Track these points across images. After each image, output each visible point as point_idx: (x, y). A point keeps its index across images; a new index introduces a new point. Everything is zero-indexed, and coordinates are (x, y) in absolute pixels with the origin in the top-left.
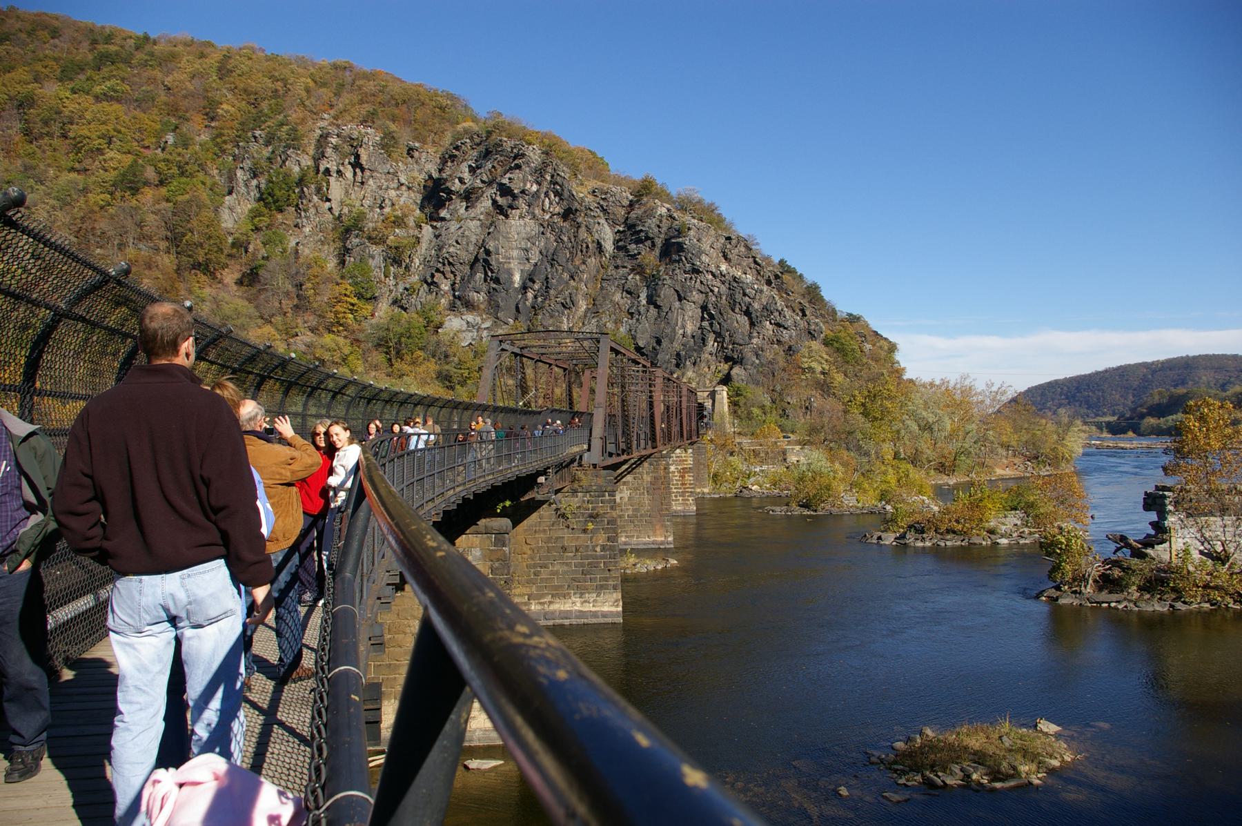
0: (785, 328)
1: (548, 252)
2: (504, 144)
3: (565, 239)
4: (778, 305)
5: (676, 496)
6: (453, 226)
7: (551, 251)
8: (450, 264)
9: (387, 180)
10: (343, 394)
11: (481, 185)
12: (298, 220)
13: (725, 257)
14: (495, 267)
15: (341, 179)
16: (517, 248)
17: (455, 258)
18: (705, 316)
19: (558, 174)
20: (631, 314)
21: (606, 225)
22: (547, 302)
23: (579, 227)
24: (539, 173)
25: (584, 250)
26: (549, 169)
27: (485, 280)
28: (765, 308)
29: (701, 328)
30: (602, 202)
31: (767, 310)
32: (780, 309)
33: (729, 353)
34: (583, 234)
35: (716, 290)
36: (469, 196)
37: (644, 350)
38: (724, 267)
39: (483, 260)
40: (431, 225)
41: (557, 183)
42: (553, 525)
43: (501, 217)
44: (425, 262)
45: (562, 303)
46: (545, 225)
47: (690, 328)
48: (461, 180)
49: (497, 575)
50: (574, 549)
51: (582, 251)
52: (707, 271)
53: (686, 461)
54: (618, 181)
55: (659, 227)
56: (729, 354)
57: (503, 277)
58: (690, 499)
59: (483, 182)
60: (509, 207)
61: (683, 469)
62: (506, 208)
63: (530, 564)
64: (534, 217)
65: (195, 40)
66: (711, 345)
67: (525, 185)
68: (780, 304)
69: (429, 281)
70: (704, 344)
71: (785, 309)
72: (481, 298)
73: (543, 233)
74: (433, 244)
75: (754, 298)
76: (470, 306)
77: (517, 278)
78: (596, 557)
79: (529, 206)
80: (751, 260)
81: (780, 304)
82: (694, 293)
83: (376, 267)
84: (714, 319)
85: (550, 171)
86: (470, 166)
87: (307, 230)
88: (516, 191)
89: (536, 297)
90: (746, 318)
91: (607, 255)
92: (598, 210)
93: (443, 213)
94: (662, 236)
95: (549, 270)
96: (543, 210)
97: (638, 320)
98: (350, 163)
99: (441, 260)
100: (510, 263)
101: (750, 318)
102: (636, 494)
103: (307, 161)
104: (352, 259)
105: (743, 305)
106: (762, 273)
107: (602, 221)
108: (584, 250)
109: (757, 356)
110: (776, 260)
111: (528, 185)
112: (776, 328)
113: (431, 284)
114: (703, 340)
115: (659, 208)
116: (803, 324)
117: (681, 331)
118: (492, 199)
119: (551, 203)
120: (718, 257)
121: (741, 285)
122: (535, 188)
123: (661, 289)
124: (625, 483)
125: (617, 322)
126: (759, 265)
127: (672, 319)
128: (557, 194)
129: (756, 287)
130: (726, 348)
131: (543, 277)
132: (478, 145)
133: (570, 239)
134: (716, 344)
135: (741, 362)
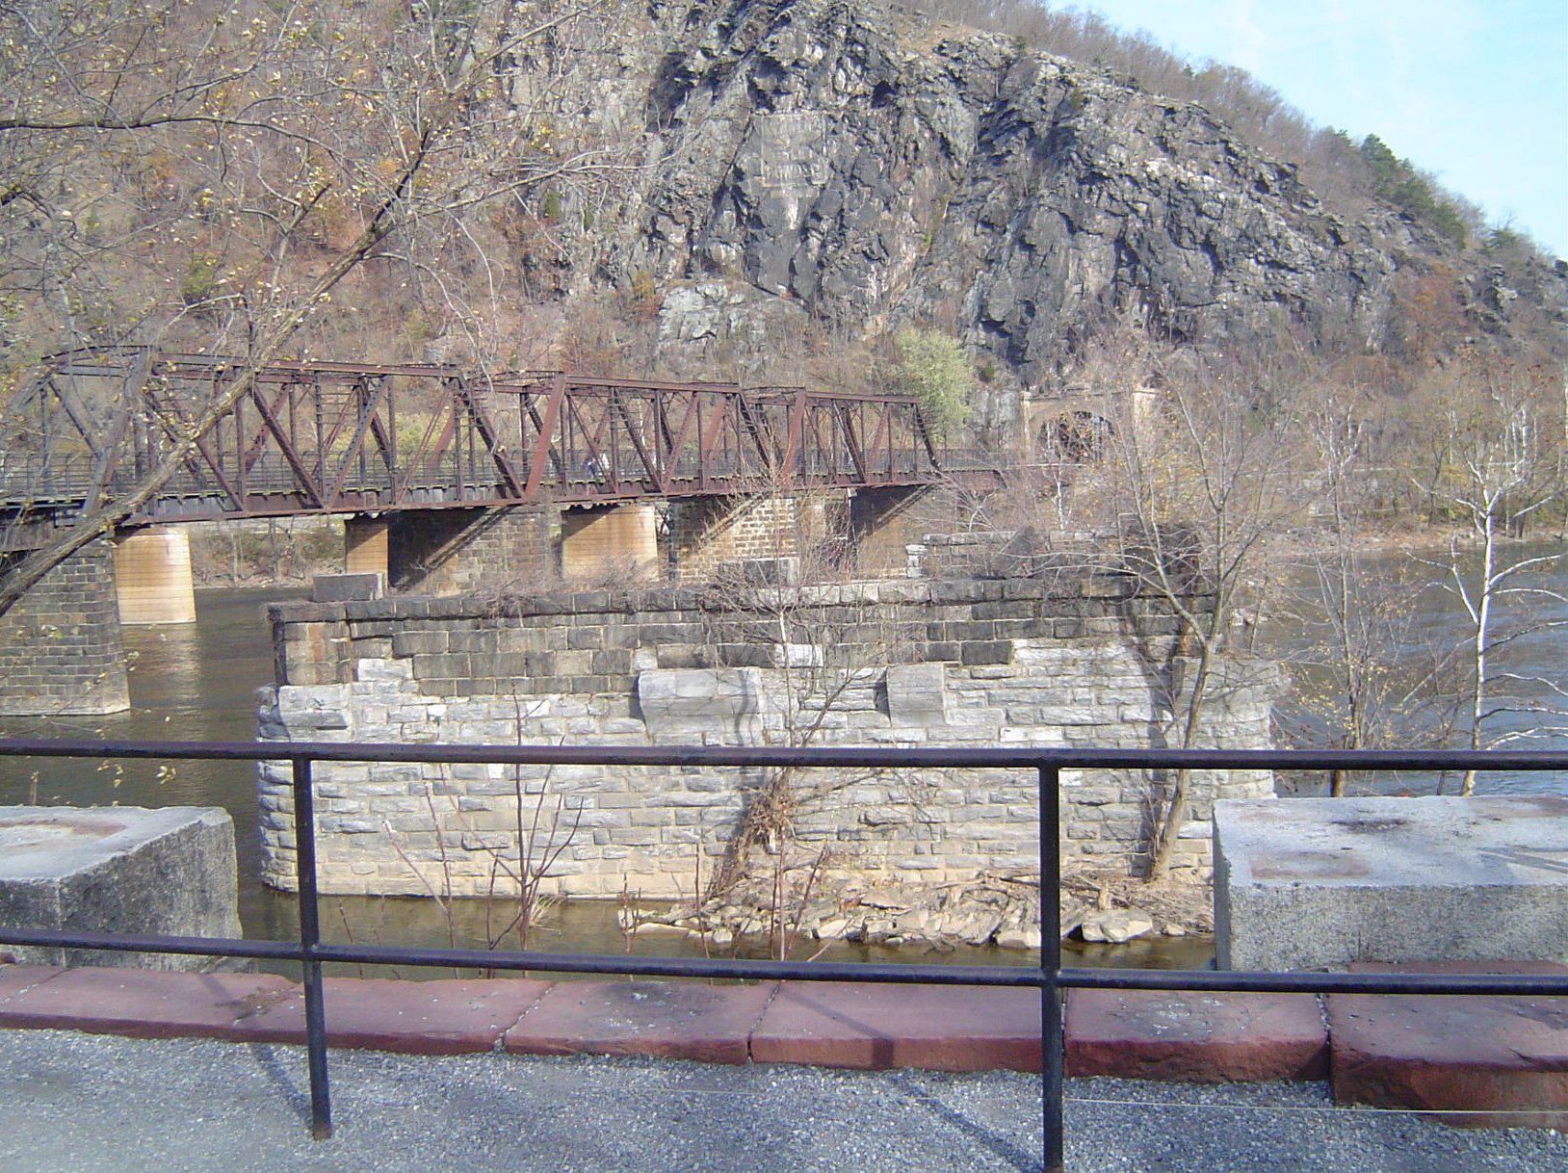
0: (1291, 270)
3: (876, 138)
4: (1270, 227)
6: (689, 131)
7: (850, 161)
13: (1164, 145)
18: (1123, 257)
19: (859, 26)
21: (958, 105)
24: (825, 27)
25: (911, 155)
26: (842, 18)
28: (1244, 235)
31: (1249, 238)
35: (1142, 208)
36: (715, 80)
37: (1005, 327)
39: (730, 191)
41: (856, 42)
45: (864, 253)
47: (1094, 280)
48: (706, 52)
52: (1121, 176)
55: (1041, 101)
57: (766, 214)
62: (770, 94)
66: (1135, 311)
67: (801, 50)
68: (1275, 223)
73: (834, 132)
76: (712, 266)
77: (793, 213)
79: (809, 86)
80: (1220, 146)
83: (571, 213)
84: (1139, 262)
85: (845, 21)
86: (721, 27)
88: (784, 64)
89: (823, 246)
90: (1207, 256)
91: (963, 160)
94: (1048, 118)
95: (847, 195)
96: (835, 90)
100: (779, 188)
101: (1214, 256)
105: (1197, 233)
106: (1241, 170)
108: (911, 155)
109: (1228, 325)
111: (808, 50)
117: (1077, 288)
119: (848, 78)
120: (1146, 147)
121: (1190, 195)
122: (819, 53)
124: (475, 553)
126: (1235, 156)
128: (857, 60)
129: (1222, 196)
131: (835, 208)
133: (883, 137)
134: (1146, 308)
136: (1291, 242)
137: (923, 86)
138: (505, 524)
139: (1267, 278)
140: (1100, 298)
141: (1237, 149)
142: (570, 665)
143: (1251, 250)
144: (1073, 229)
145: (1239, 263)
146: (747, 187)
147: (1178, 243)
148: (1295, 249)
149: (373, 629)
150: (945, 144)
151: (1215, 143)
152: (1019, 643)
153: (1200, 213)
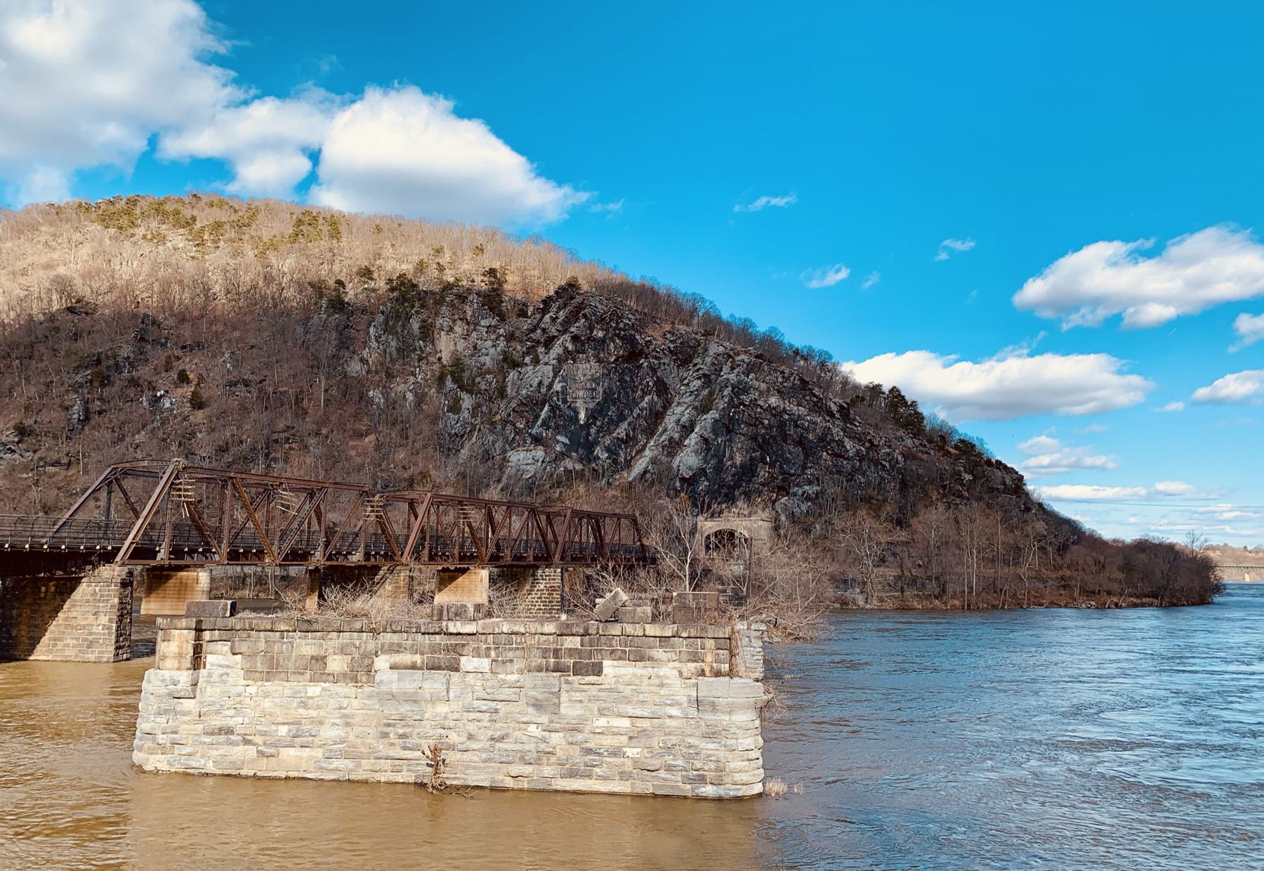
0: (845, 459)
5: (544, 613)
16: (583, 389)
29: (752, 459)
35: (766, 422)
61: (551, 587)
64: (599, 361)
65: (512, 282)
67: (592, 332)
78: (99, 634)
86: (551, 317)
111: (595, 332)
119: (615, 348)
139: (833, 462)
142: (336, 664)
143: (825, 446)
148: (848, 448)
149: (211, 636)
152: (606, 663)
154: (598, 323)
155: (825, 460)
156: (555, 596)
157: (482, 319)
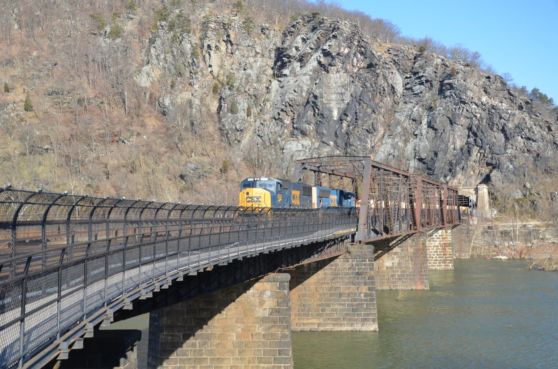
0: (534, 141)
1: (356, 94)
2: (325, 22)
3: (368, 85)
4: (528, 124)
5: (439, 263)
7: (359, 93)
8: (290, 105)
9: (248, 51)
10: (163, 209)
11: (310, 51)
12: (191, 80)
13: (486, 92)
14: (320, 107)
15: (218, 52)
16: (335, 93)
17: (293, 102)
19: (363, 40)
20: (416, 135)
22: (357, 129)
23: (378, 76)
24: (349, 40)
25: (382, 92)
26: (357, 37)
27: (314, 115)
28: (517, 127)
29: (468, 143)
30: (394, 58)
32: (529, 127)
33: (489, 161)
34: (381, 81)
35: (478, 115)
38: (484, 99)
40: (277, 80)
42: (333, 279)
43: (324, 72)
44: (274, 105)
45: (367, 130)
46: (354, 77)
47: (459, 144)
48: (297, 48)
49: (280, 306)
50: (347, 295)
51: (380, 93)
53: (447, 238)
54: (405, 41)
55: (436, 72)
56: (489, 161)
57: (326, 113)
58: (450, 265)
59: (311, 49)
60: (329, 65)
61: (445, 244)
62: (327, 66)
63: (319, 304)
64: (346, 71)
67: (340, 49)
68: (529, 123)
69: (277, 118)
70: (469, 154)
71: (534, 127)
72: (311, 128)
73: (353, 82)
74: (279, 92)
75: (508, 120)
76: (304, 134)
77: (336, 114)
78: (361, 300)
80: (506, 92)
81: (529, 123)
82: (462, 119)
83: (241, 109)
85: (357, 38)
87: (196, 87)
88: (333, 54)
89: (348, 126)
90: (502, 135)
92: (392, 64)
93: (286, 71)
97: (420, 139)
98: (224, 41)
99: (284, 103)
101: (505, 135)
102: (403, 261)
103: (195, 40)
104: (226, 105)
105: (499, 125)
106: (515, 101)
107: (395, 71)
109: (511, 161)
110: (529, 90)
111: (342, 50)
112: (526, 141)
113: (278, 119)
114: (469, 152)
115: (436, 59)
116: (549, 137)
117: (452, 146)
118: (318, 60)
119: (358, 61)
120: (479, 91)
121: (498, 111)
122: (346, 51)
123: (437, 117)
124: (395, 253)
125: (406, 141)
127: (445, 138)
128: (362, 53)
129: (509, 111)
130: (487, 157)
131: (354, 112)
132: (309, 22)
133: (371, 85)
135: (499, 167)
136: (534, 129)
137: (385, 65)
138: (409, 241)
140: (462, 149)
141: (513, 93)
144: (451, 123)
145: (515, 137)
146: (318, 103)
147: (492, 129)
150: (393, 88)
151: (504, 90)
153: (501, 118)
154: (344, 42)
155: (520, 143)
156: (447, 250)
157: (242, 40)
